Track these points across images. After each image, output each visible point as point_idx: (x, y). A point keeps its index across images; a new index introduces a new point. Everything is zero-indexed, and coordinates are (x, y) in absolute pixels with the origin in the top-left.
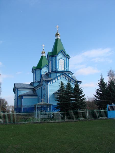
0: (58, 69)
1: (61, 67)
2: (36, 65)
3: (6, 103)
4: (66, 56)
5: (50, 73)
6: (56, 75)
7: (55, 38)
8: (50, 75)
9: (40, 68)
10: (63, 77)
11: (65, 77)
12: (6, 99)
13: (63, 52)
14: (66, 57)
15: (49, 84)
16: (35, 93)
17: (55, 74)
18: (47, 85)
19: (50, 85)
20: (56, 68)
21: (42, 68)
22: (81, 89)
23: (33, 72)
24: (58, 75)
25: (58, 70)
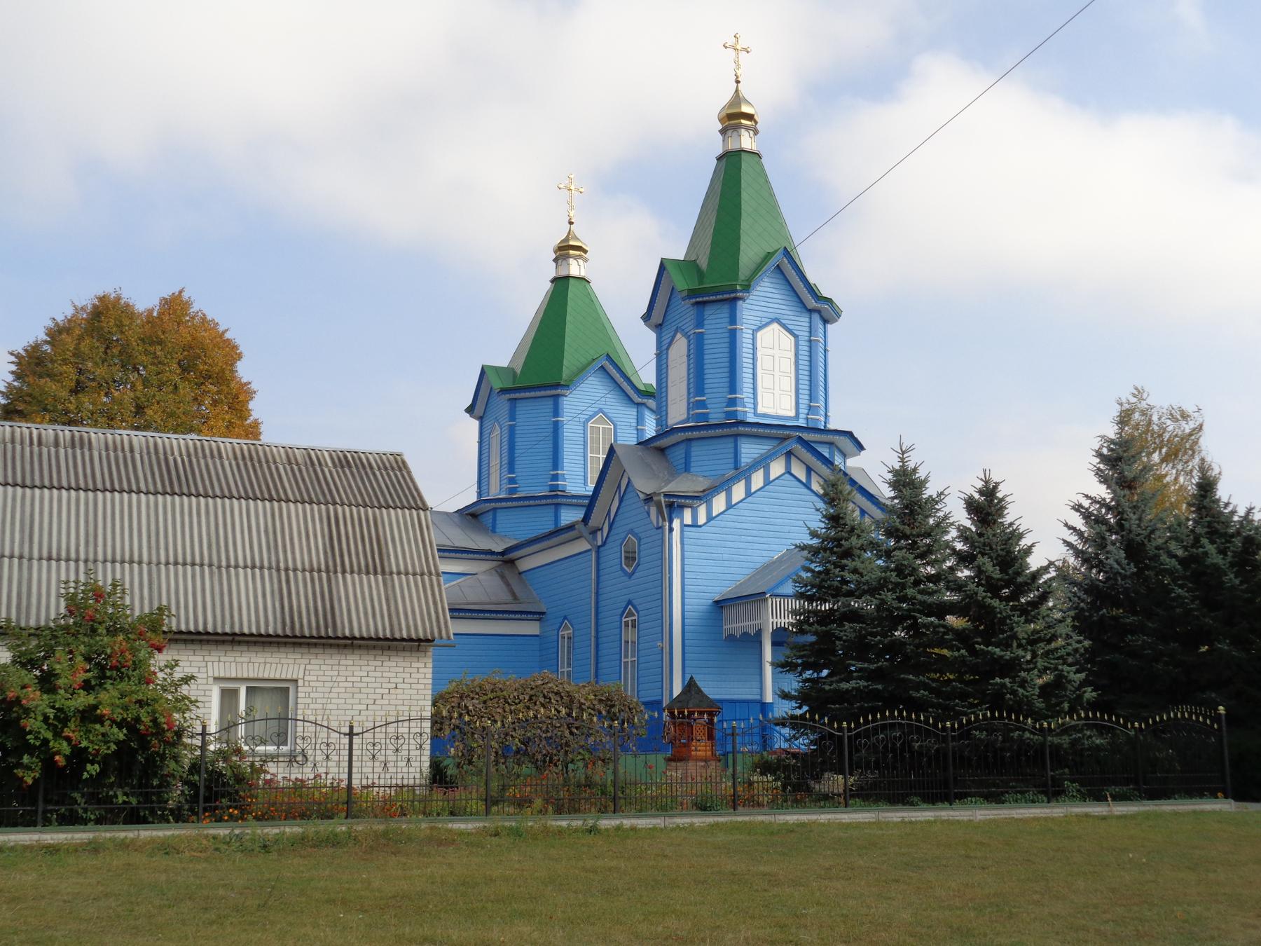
0: (749, 409)
1: (773, 392)
2: (504, 347)
4: (812, 303)
6: (557, 518)
7: (551, 271)
8: (494, 520)
9: (557, 386)
10: (789, 472)
11: (802, 475)
12: (257, 397)
14: (638, 404)
15: (683, 526)
18: (671, 530)
19: (690, 533)
20: (733, 402)
21: (567, 387)
22: (1073, 539)
23: (479, 409)
24: (750, 451)
25: (751, 418)
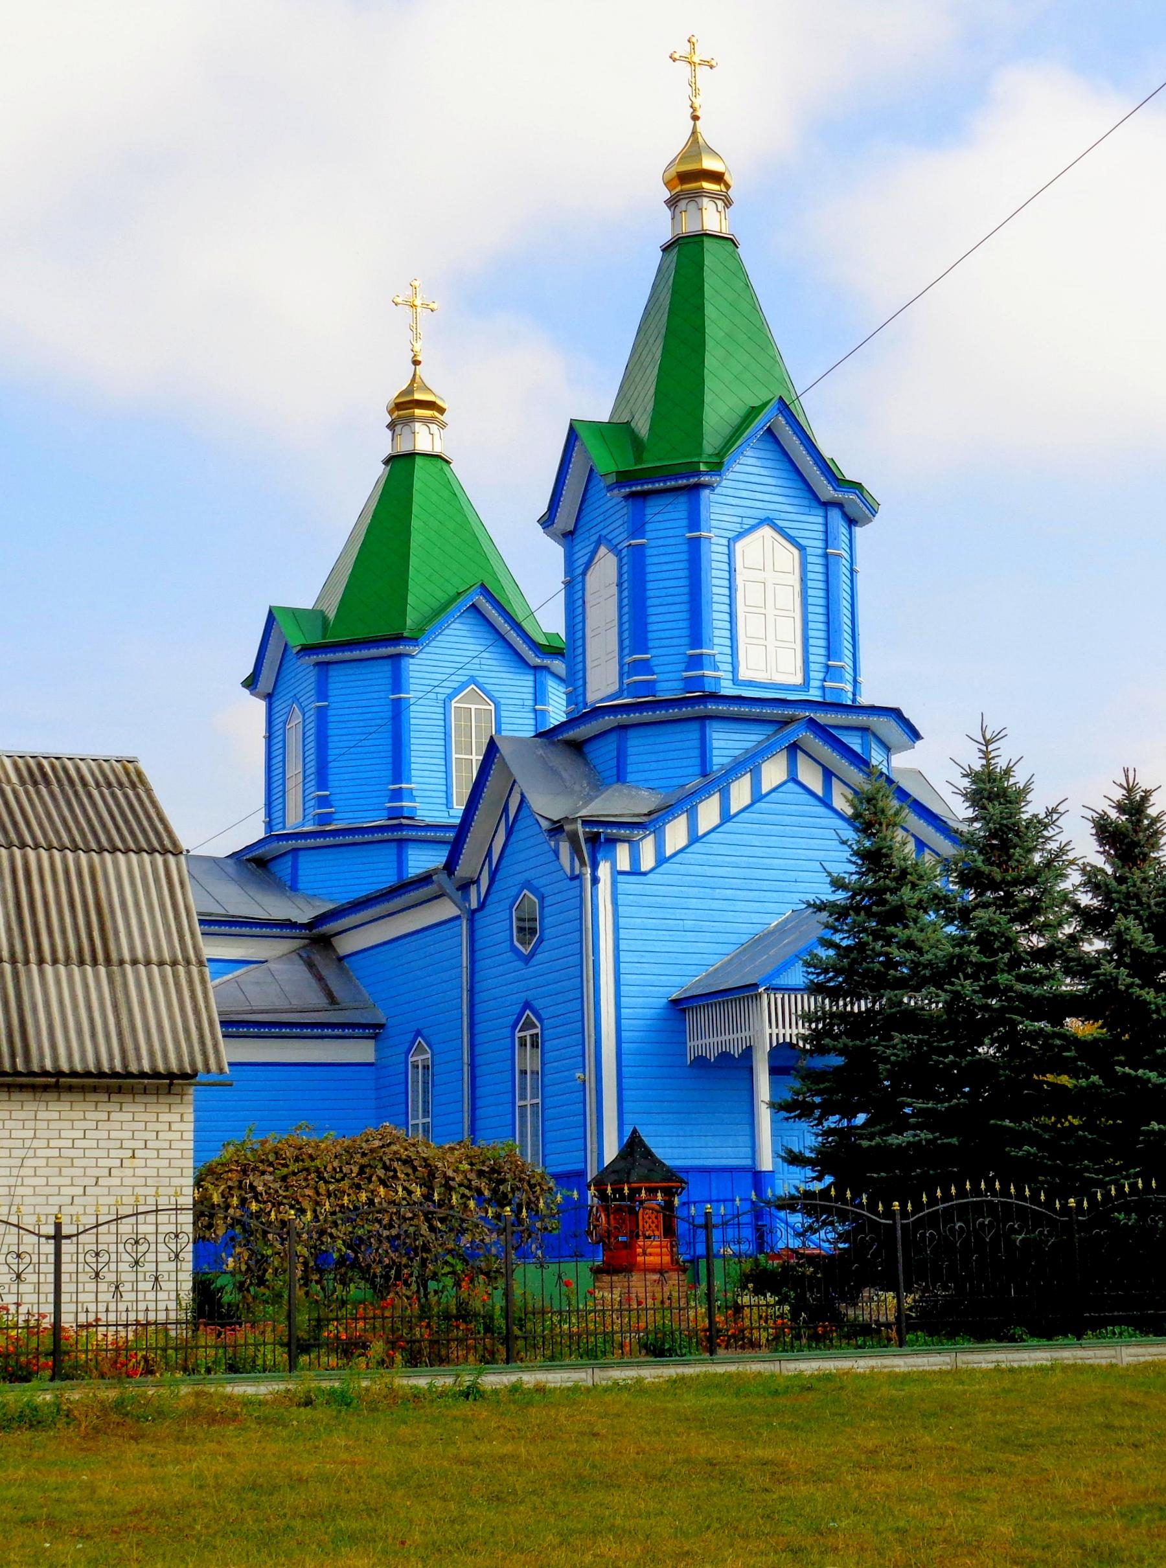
0: (724, 673)
1: (764, 647)
2: (307, 579)
3: (1155, 846)
4: (828, 491)
5: (609, 721)
10: (793, 779)
13: (783, 433)
15: (616, 873)
16: (335, 985)
17: (689, 736)
18: (595, 881)
19: (628, 885)
20: (696, 662)
21: (414, 640)
23: (266, 683)
24: (727, 744)
